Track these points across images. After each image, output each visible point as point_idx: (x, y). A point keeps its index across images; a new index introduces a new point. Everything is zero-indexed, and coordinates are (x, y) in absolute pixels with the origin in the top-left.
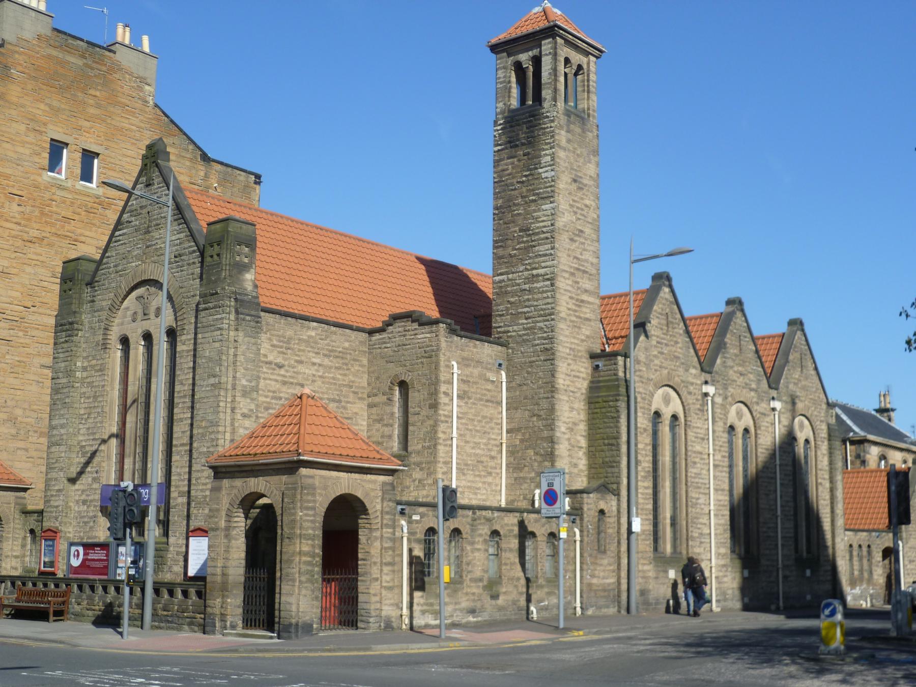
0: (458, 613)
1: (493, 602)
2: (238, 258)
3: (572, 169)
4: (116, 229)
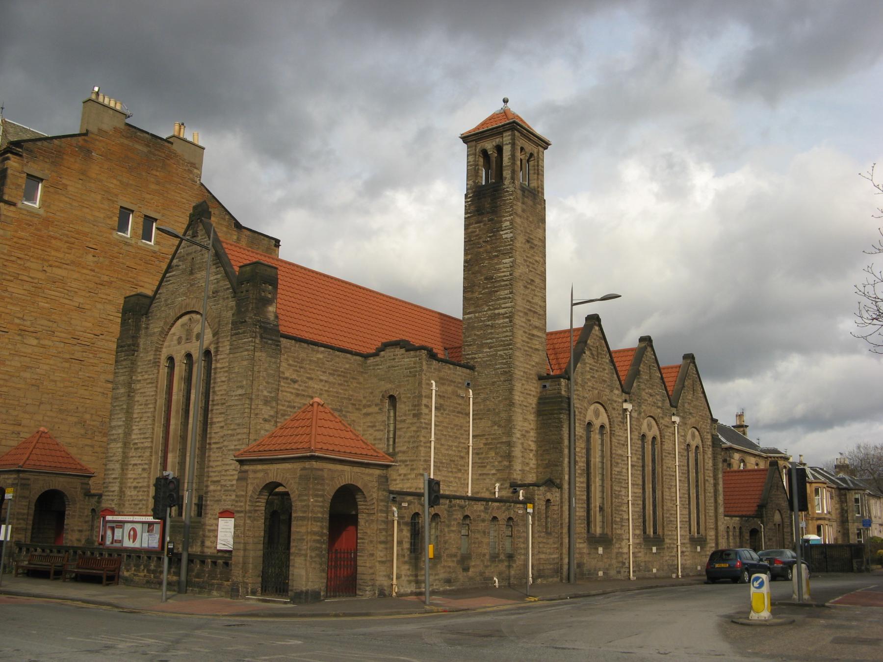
0: (437, 582)
1: (465, 574)
2: (263, 294)
3: (526, 232)
4: (167, 271)
